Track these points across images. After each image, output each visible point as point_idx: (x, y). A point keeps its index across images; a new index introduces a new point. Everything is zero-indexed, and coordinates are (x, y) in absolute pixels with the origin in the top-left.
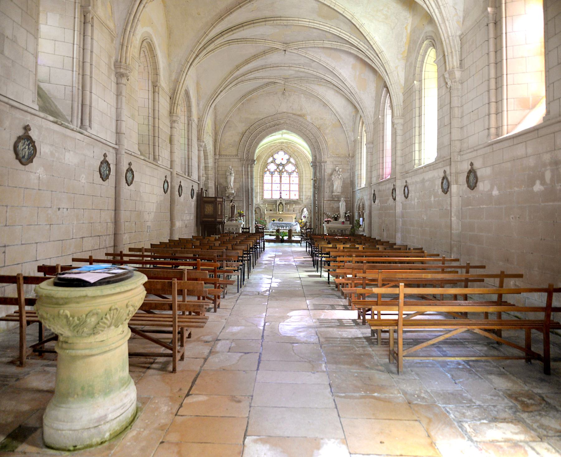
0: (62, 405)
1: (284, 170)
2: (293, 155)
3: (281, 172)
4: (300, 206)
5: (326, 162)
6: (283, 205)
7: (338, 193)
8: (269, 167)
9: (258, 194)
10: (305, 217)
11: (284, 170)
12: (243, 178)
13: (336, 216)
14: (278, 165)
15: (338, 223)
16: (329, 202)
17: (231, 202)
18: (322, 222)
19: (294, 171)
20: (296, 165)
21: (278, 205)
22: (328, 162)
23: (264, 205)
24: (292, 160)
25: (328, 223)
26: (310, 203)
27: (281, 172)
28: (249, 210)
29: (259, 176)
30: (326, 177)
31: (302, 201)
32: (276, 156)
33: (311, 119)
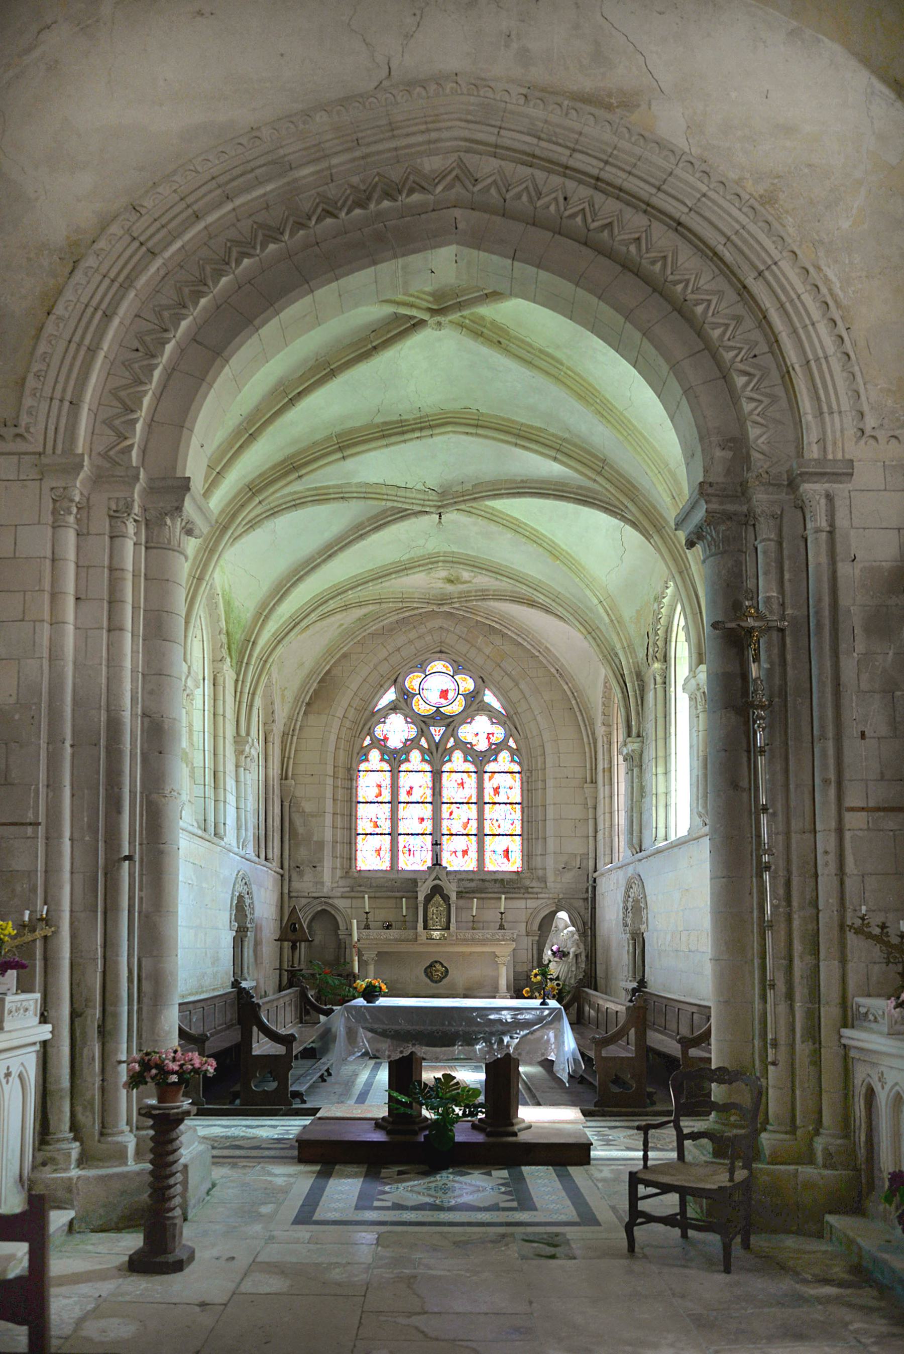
0: (895, 564)
1: (451, 743)
4: (531, 904)
6: (446, 898)
8: (379, 731)
9: (328, 851)
10: (561, 954)
11: (451, 743)
12: (56, 623)
14: (423, 723)
18: (829, 1013)
19: (502, 746)
21: (421, 897)
29: (330, 771)
31: (543, 880)
32: (413, 682)
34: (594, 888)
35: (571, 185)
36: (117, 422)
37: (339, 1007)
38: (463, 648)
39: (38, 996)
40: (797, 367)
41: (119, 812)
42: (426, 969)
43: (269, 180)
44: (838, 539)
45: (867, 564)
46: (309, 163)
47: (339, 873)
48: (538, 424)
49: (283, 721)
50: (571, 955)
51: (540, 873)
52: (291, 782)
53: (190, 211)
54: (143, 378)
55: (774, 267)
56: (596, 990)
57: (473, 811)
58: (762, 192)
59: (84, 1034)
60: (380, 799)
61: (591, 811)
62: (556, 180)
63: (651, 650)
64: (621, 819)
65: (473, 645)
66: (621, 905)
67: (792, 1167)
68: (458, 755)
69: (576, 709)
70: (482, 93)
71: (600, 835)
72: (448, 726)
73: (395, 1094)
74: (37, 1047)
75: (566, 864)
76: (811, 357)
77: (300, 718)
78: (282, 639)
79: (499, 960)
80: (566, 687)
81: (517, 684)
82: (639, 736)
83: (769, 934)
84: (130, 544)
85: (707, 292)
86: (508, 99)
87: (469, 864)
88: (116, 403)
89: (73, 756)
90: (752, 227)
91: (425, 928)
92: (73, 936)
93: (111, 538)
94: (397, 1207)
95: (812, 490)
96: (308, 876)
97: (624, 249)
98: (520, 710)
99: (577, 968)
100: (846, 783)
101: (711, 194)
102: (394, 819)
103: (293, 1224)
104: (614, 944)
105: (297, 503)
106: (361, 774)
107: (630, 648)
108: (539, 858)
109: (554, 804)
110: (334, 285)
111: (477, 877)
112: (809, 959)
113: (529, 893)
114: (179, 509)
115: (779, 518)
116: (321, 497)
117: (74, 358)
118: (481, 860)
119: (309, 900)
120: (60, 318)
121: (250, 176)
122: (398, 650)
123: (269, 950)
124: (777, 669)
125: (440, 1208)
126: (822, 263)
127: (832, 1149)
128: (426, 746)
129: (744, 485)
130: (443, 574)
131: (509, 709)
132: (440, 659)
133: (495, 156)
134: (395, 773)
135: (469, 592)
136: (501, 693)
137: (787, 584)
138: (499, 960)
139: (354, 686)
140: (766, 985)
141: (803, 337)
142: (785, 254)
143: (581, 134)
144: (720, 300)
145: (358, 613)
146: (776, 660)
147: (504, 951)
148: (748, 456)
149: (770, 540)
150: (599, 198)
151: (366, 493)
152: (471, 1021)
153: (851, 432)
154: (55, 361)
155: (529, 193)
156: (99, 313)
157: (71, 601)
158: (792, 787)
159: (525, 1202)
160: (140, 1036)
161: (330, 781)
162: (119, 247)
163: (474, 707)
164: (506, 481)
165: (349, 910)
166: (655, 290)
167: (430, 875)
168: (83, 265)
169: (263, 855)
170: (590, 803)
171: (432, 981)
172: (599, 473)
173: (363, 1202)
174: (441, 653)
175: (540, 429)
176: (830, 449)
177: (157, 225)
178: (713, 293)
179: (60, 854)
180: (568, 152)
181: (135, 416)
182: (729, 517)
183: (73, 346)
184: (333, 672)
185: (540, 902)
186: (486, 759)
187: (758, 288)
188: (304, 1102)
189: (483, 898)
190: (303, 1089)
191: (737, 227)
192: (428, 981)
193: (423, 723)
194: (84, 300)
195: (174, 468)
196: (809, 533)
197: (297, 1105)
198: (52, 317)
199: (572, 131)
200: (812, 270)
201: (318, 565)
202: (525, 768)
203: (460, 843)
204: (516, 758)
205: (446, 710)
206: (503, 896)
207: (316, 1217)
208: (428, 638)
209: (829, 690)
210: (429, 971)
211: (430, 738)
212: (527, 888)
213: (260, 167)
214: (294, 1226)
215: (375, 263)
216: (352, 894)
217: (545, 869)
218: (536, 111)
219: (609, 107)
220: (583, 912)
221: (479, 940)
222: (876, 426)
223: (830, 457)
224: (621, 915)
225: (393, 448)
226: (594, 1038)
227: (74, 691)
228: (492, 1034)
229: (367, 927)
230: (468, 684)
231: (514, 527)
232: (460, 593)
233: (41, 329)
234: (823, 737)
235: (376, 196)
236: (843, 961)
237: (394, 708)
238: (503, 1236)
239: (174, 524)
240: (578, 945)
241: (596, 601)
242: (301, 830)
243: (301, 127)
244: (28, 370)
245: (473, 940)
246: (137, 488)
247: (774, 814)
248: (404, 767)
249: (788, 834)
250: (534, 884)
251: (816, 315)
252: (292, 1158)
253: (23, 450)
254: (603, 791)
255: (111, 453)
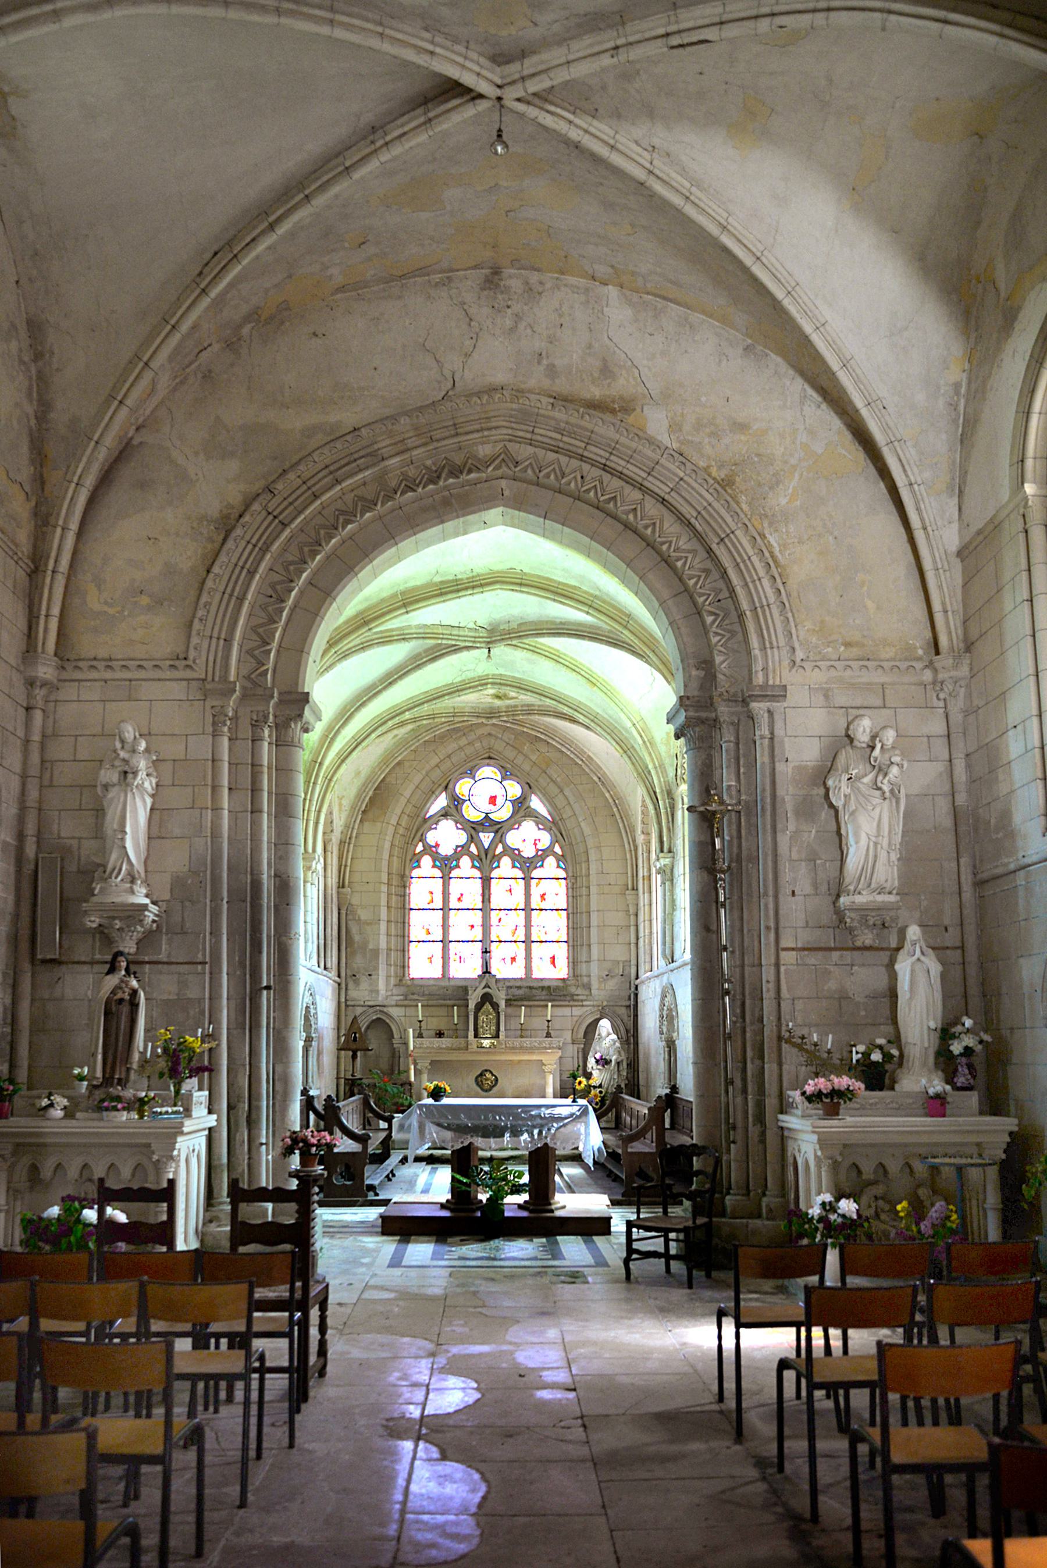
1: (500, 849)
2: (543, 781)
3: (486, 861)
4: (577, 1011)
5: (780, 694)
6: (495, 1006)
7: (881, 891)
8: (431, 837)
9: (382, 958)
10: (603, 1062)
11: (500, 849)
12: (216, 809)
13: (876, 1056)
14: (473, 829)
15: (900, 1110)
16: (812, 959)
17: (112, 970)
18: (771, 1102)
20: (555, 826)
21: (472, 1005)
22: (796, 696)
23: (410, 1011)
24: (536, 803)
25: (832, 1112)
26: (625, 994)
27: (486, 861)
28: (255, 1026)
29: (384, 877)
30: (788, 794)
31: (588, 987)
32: (462, 787)
33: (674, 427)
34: (636, 995)
35: (586, 467)
36: (256, 652)
37: (400, 1115)
38: (510, 753)
39: (207, 1093)
40: (748, 613)
41: (260, 952)
42: (477, 1078)
43: (367, 468)
44: (777, 745)
45: (797, 764)
46: (397, 454)
47: (393, 981)
48: (573, 582)
49: (340, 829)
50: (613, 1063)
51: (585, 980)
52: (347, 890)
53: (310, 492)
54: (276, 618)
55: (732, 535)
56: (639, 1098)
57: (520, 917)
58: (723, 476)
59: (237, 1122)
60: (431, 906)
61: (632, 918)
62: (575, 463)
63: (679, 771)
64: (657, 927)
65: (520, 752)
66: (658, 1014)
67: (744, 1221)
68: (506, 861)
69: (618, 817)
70: (521, 401)
71: (641, 941)
72: (496, 832)
73: (458, 1177)
74: (206, 1132)
75: (609, 971)
76: (758, 605)
77: (356, 827)
78: (347, 757)
79: (546, 1068)
80: (607, 795)
81: (562, 791)
82: (670, 851)
83: (729, 1043)
84: (266, 744)
85: (684, 551)
86: (539, 405)
87: (516, 972)
88: (255, 637)
89: (228, 909)
90: (715, 504)
91: (476, 1036)
92: (229, 1048)
93: (253, 741)
94: (461, 1258)
95: (758, 707)
96: (364, 984)
97: (624, 517)
98: (564, 816)
99: (619, 1075)
100: (781, 930)
101: (686, 478)
102: (445, 926)
103: (389, 1266)
104: (653, 1052)
105: (363, 648)
106: (413, 880)
107: (661, 767)
108: (584, 965)
109: (598, 911)
110: (414, 538)
111: (525, 984)
112: (758, 1062)
113: (574, 1000)
114: (300, 716)
115: (736, 725)
116: (386, 639)
117: (227, 606)
118: (528, 967)
119: (365, 1009)
120: (216, 575)
121: (354, 465)
122: (449, 756)
123: (328, 1060)
124: (735, 841)
125: (494, 1259)
126: (766, 532)
127: (772, 1206)
128: (475, 852)
129: (711, 698)
130: (491, 691)
131: (554, 813)
132: (488, 765)
133: (531, 444)
134: (446, 879)
135: (516, 706)
136: (549, 800)
137: (742, 776)
138: (546, 1068)
139: (407, 793)
140: (729, 1082)
141: (753, 591)
142: (740, 525)
143: (592, 432)
144: (694, 557)
145: (410, 727)
146: (735, 833)
147: (551, 1060)
148: (715, 676)
149: (730, 742)
150: (606, 477)
151: (424, 633)
152: (517, 1116)
153: (786, 663)
154: (213, 609)
155: (555, 473)
156: (245, 571)
157: (226, 791)
158: (745, 931)
159: (556, 1254)
160: (274, 1125)
161: (384, 888)
162: (259, 519)
163: (522, 813)
164: (547, 622)
165: (403, 1019)
166: (648, 545)
167: (480, 983)
168: (233, 535)
169: (322, 965)
170: (632, 910)
171: (483, 1090)
172: (626, 627)
173: (435, 1256)
174: (490, 759)
175: (575, 587)
176: (771, 677)
177: (286, 503)
178: (689, 552)
179: (220, 986)
180: (583, 445)
181: (269, 647)
182: (702, 721)
183: (226, 596)
184: (388, 780)
185: (585, 1009)
186: (533, 865)
187: (720, 552)
188: (377, 1195)
189: (530, 1006)
190: (376, 1183)
191: (705, 504)
192: (478, 1089)
193: (473, 829)
194: (234, 560)
195: (297, 684)
196: (757, 738)
197: (371, 1196)
198: (211, 575)
199: (587, 430)
200: (758, 538)
201: (380, 692)
202: (570, 874)
203: (509, 950)
204: (561, 864)
205: (493, 816)
206: (550, 1004)
207: (403, 1264)
208: (478, 745)
209: (770, 858)
210: (479, 1079)
211: (479, 844)
212: (573, 995)
213: (363, 457)
214: (391, 1269)
215: (442, 522)
216: (406, 1003)
217: (589, 976)
218: (559, 415)
219: (613, 411)
220: (625, 1018)
221: (526, 1048)
222: (804, 657)
223: (771, 682)
224: (658, 1023)
225: (448, 603)
226: (621, 1135)
227: (228, 861)
228: (534, 1127)
229: (420, 1036)
230: (514, 789)
231: (556, 658)
232: (507, 707)
233: (203, 583)
234: (766, 894)
235: (444, 475)
236: (780, 1065)
237: (445, 814)
238: (539, 1273)
239: (296, 726)
240: (619, 1052)
241: (629, 725)
242: (357, 938)
243: (390, 427)
244: (194, 617)
245: (521, 1048)
246: (272, 703)
247: (733, 952)
248: (454, 873)
249: (743, 966)
250: (579, 991)
251: (762, 573)
252: (377, 1233)
253: (191, 677)
254: (643, 899)
255: (253, 676)
